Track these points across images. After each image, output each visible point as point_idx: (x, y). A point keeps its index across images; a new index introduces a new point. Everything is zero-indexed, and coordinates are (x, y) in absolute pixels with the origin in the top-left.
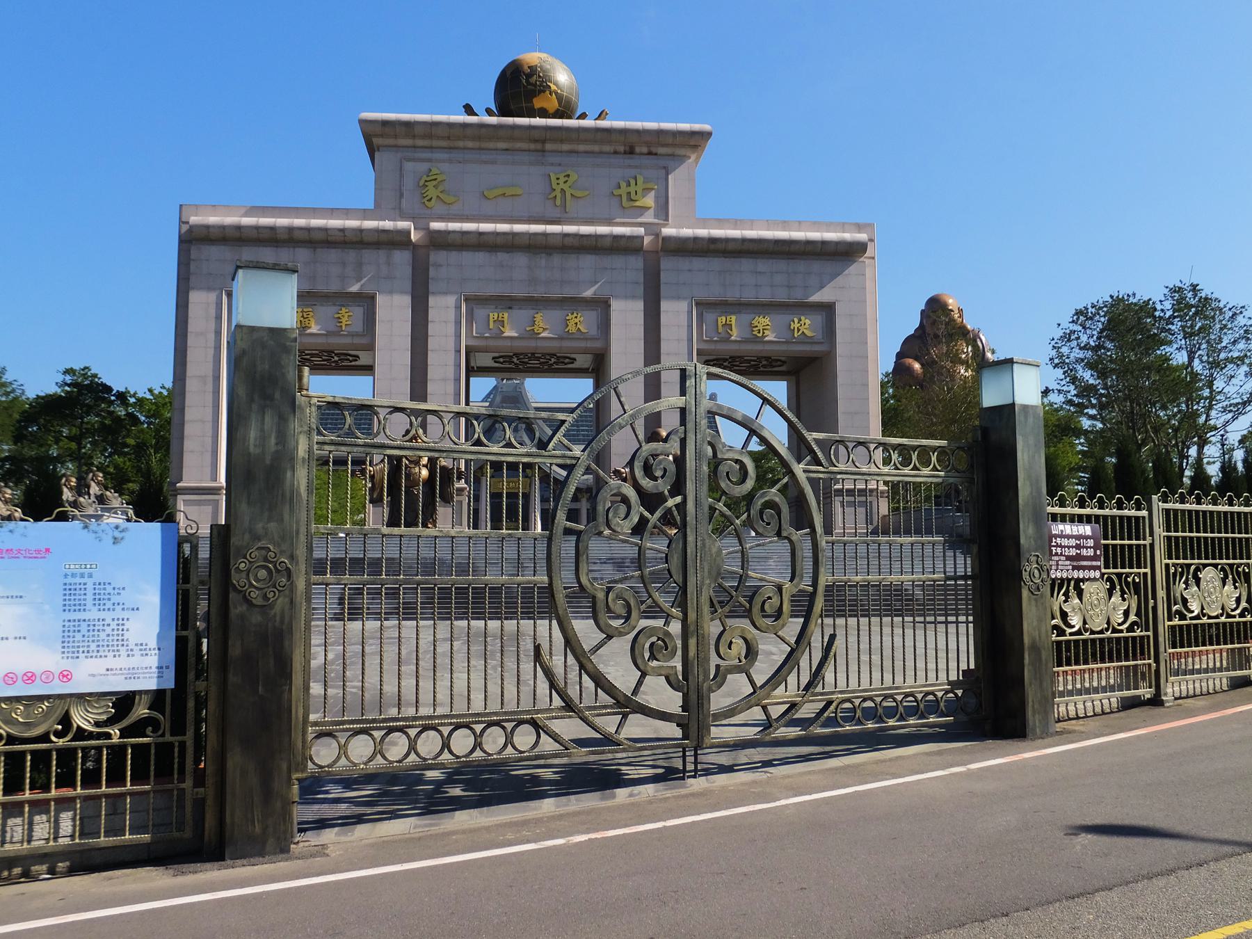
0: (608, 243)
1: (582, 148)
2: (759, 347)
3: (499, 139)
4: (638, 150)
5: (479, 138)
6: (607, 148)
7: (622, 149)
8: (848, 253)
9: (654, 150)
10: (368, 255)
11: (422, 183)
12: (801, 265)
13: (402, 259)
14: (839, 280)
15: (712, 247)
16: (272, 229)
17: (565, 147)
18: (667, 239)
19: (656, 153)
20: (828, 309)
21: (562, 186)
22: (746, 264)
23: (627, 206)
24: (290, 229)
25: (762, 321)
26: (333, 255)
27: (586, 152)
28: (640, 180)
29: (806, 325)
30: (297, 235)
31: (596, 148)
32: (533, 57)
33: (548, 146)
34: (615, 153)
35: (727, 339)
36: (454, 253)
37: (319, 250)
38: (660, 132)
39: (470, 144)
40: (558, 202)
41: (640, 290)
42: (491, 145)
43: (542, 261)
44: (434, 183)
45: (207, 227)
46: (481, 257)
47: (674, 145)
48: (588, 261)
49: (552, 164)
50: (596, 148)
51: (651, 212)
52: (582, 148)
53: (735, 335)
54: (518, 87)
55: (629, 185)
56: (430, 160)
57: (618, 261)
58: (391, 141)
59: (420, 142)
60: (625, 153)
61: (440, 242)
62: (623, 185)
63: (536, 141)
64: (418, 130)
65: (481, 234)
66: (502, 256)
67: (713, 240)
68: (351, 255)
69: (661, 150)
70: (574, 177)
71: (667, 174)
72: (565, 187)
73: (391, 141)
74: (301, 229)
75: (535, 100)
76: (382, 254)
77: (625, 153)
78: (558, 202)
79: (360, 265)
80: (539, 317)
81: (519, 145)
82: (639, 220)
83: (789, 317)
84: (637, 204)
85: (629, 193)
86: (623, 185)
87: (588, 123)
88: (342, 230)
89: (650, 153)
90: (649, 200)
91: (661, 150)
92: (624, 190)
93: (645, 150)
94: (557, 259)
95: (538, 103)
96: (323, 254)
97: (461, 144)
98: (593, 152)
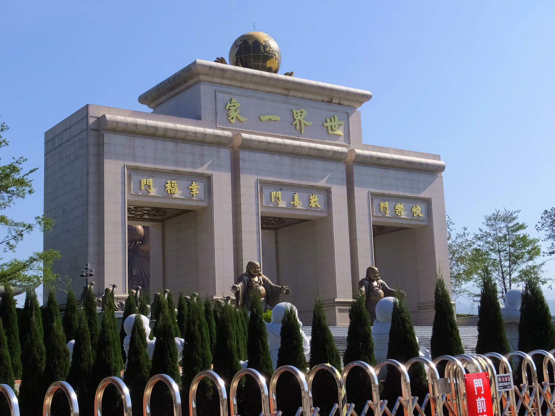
0: (330, 154)
1: (307, 96)
2: (397, 221)
3: (267, 85)
4: (334, 101)
5: (256, 83)
6: (319, 98)
7: (326, 99)
8: (434, 171)
9: (342, 102)
10: (207, 150)
11: (227, 108)
12: (415, 176)
13: (225, 153)
14: (432, 186)
15: (378, 162)
16: (156, 128)
17: (300, 95)
18: (358, 156)
19: (341, 103)
20: (428, 202)
21: (299, 118)
22: (392, 173)
23: (328, 134)
24: (166, 130)
25: (400, 207)
26: (187, 148)
27: (308, 99)
28: (336, 118)
29: (419, 210)
30: (169, 134)
31: (314, 97)
32: (264, 36)
33: (291, 93)
34: (323, 101)
35: (384, 216)
36: (252, 153)
37: (179, 144)
38: (348, 93)
39: (251, 86)
40: (298, 127)
41: (345, 182)
42: (262, 88)
43: (297, 162)
44: (235, 108)
45: (117, 122)
46: (266, 157)
47: (352, 101)
48: (319, 164)
49: (293, 104)
50: (314, 97)
51: (342, 138)
52: (307, 96)
53: (153, 192)
54: (249, 51)
55: (331, 121)
56: (230, 93)
57: (333, 166)
58: (209, 79)
59: (225, 82)
60: (328, 102)
61: (248, 146)
62: (329, 120)
63: (286, 89)
64: (228, 75)
65: (269, 143)
66: (277, 158)
67: (379, 158)
68: (197, 149)
69: (345, 103)
70: (305, 113)
71: (348, 117)
72: (301, 118)
73: (209, 79)
74: (172, 130)
75: (268, 62)
76: (214, 149)
77: (328, 102)
78: (298, 127)
79: (202, 156)
80: (296, 196)
81: (277, 90)
82: (336, 142)
83: (411, 205)
84: (336, 133)
85: (332, 126)
86: (329, 120)
87: (280, 76)
88: (195, 133)
89: (339, 104)
90: (340, 132)
91: (345, 103)
92: (328, 124)
93: (338, 101)
94: (304, 162)
95: (269, 64)
96: (181, 146)
97: (246, 85)
98: (311, 99)
